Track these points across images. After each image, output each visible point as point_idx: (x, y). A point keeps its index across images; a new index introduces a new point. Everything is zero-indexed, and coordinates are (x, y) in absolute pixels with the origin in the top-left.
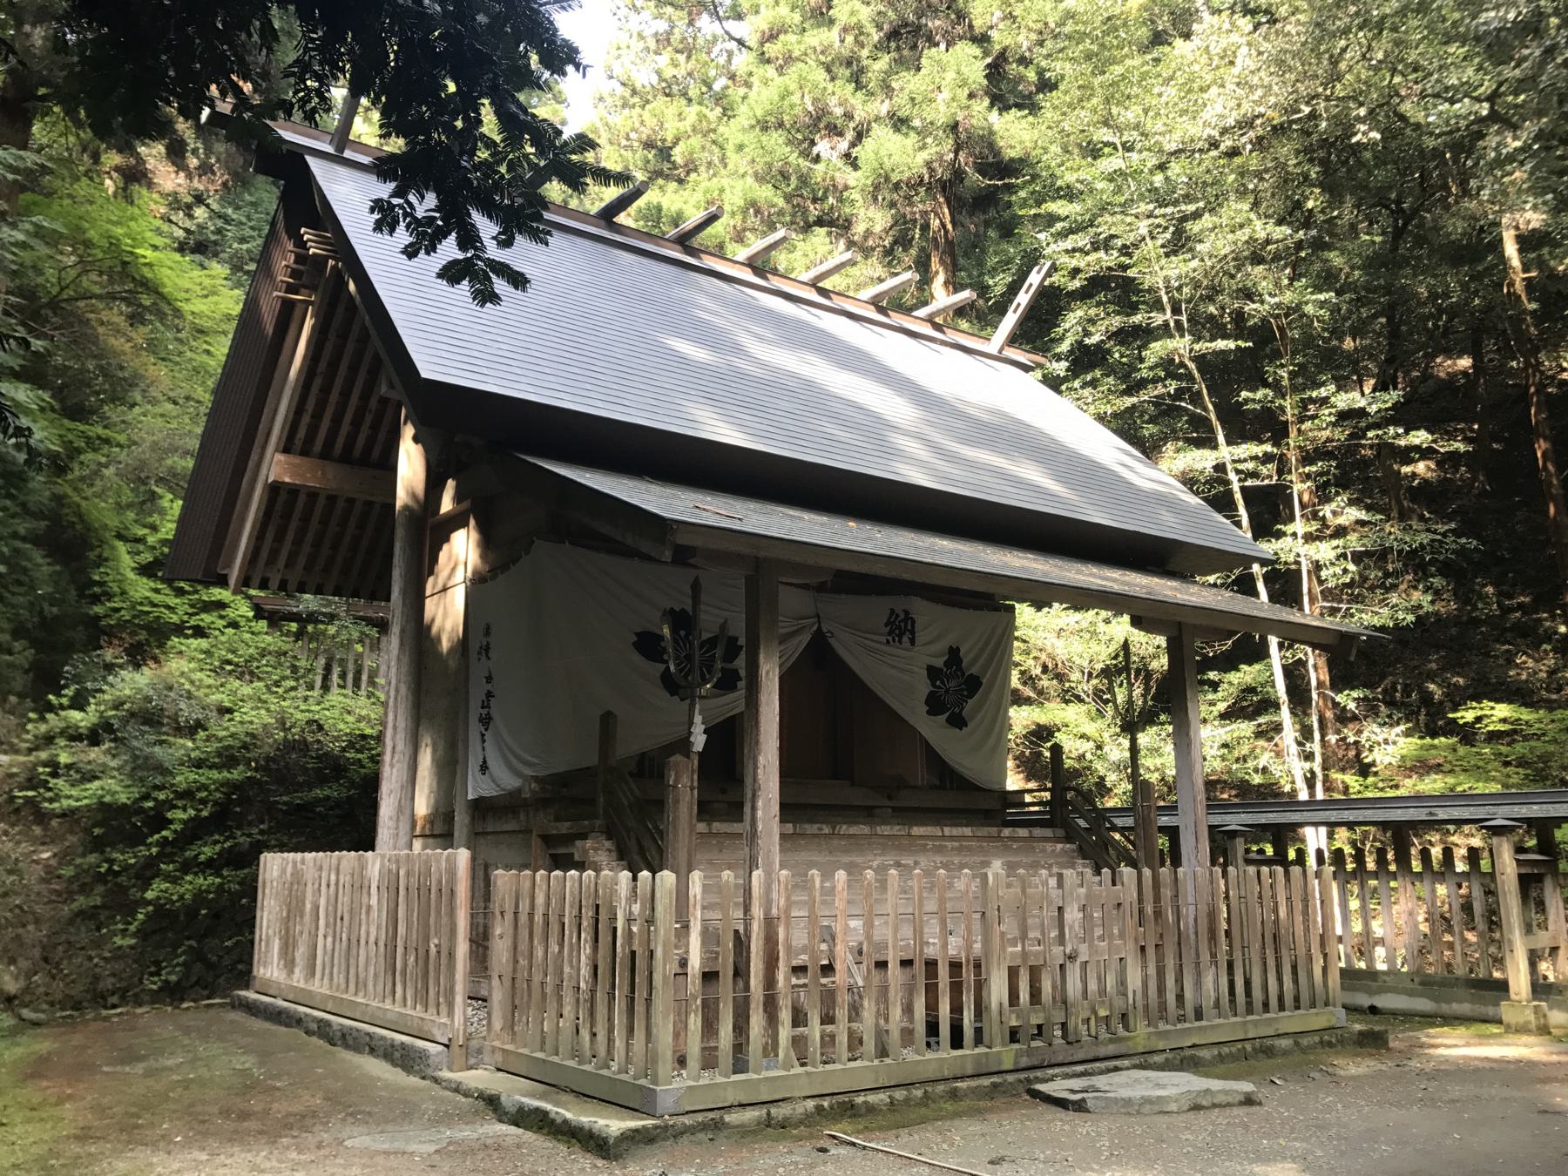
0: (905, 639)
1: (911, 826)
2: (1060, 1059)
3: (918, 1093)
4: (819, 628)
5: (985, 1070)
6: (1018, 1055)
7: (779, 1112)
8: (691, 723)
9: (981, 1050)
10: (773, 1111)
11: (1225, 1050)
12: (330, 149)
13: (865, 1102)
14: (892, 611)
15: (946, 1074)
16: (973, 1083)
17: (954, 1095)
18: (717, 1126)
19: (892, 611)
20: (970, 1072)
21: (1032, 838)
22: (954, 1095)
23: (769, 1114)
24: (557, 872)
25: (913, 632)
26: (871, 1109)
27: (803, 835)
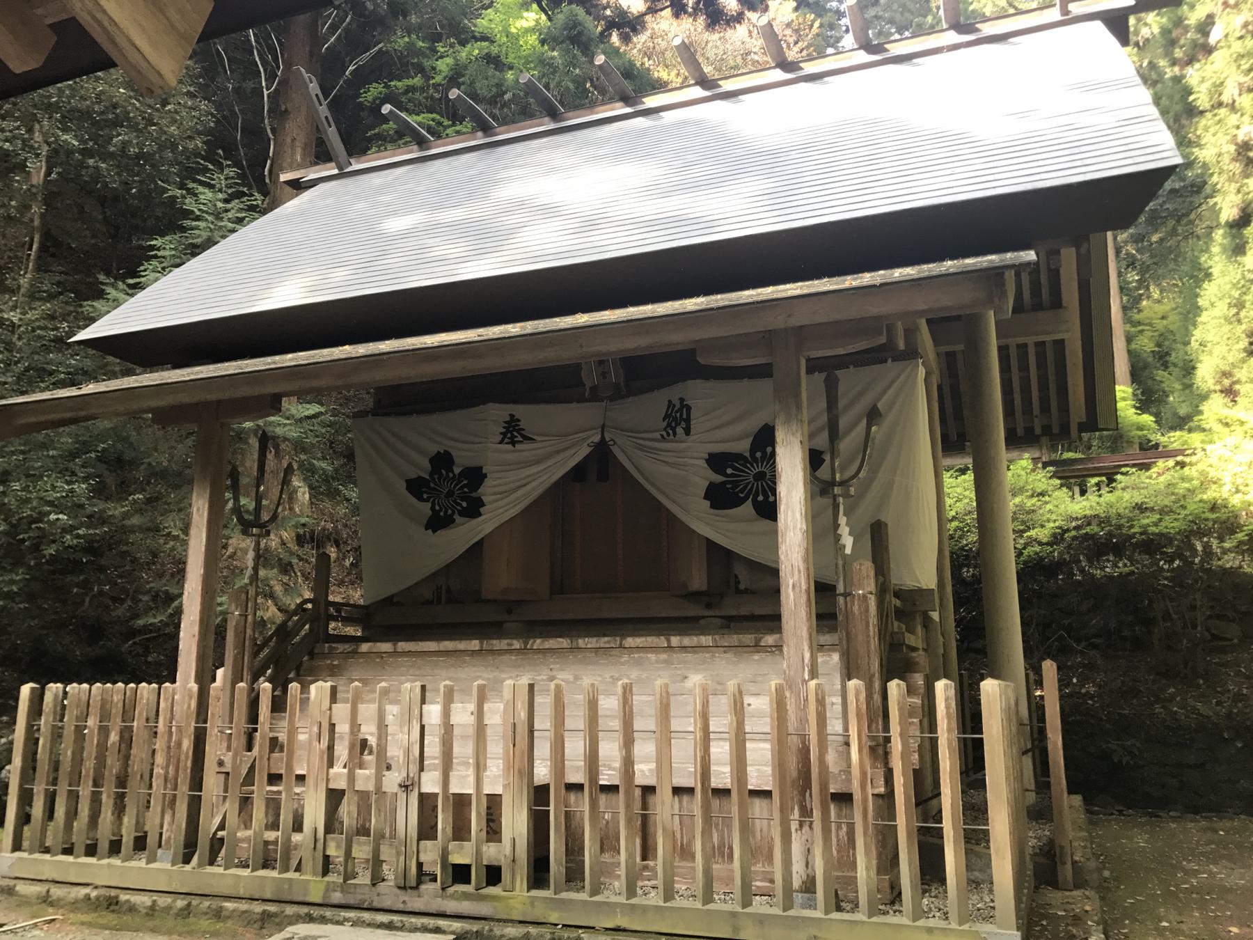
0: (679, 430)
1: (623, 636)
2: (387, 904)
3: (181, 903)
4: (603, 437)
5: (284, 898)
6: (328, 889)
7: (57, 892)
8: (836, 526)
9: (297, 874)
10: (194, 903)
11: (57, 892)
12: (336, 171)
13: (128, 901)
14: (670, 401)
15: (241, 893)
16: (243, 906)
17: (218, 914)
18: (10, 891)
19: (670, 401)
20: (268, 896)
21: (395, 653)
22: (218, 914)
23: (154, 901)
24: (132, 685)
25: (688, 421)
26: (132, 909)
27: (492, 652)
